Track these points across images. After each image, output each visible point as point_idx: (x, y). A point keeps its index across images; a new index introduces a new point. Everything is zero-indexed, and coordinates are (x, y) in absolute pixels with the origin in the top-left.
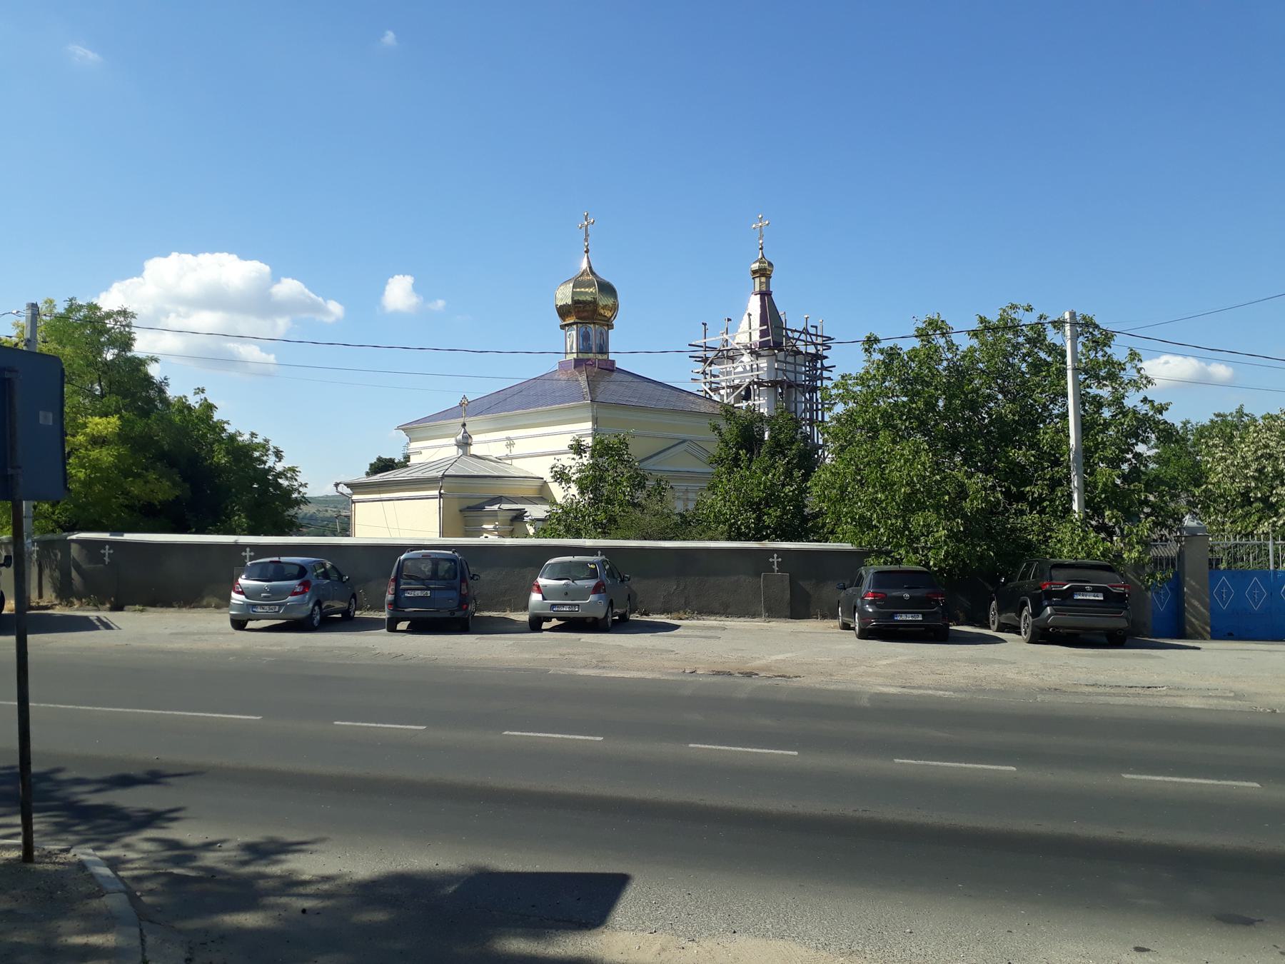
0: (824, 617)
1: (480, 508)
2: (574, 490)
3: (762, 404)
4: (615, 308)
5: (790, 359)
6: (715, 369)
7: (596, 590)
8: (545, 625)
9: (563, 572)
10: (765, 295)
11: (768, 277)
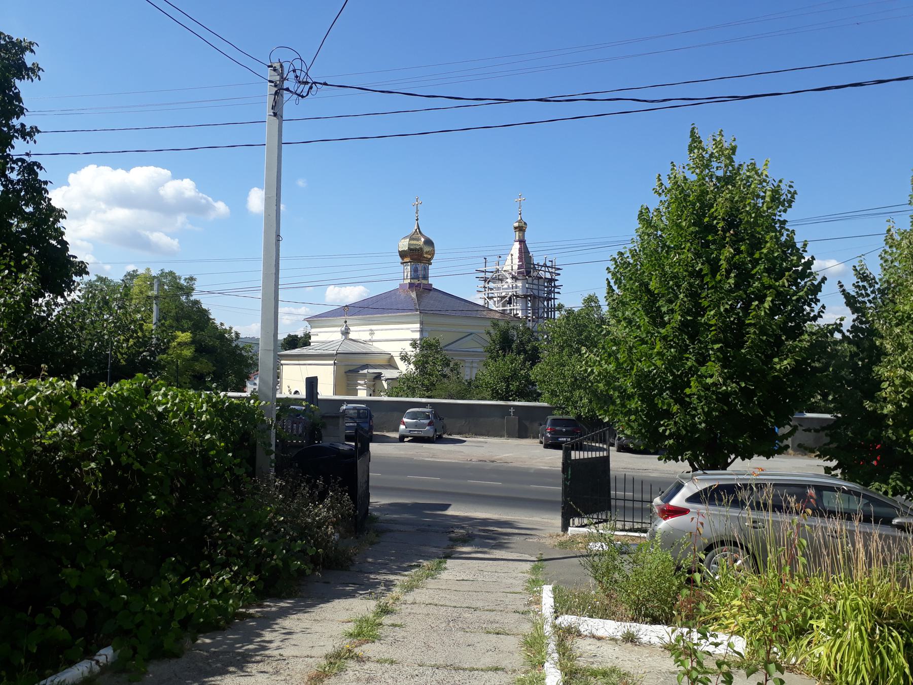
0: (534, 438)
1: (356, 371)
2: (412, 366)
3: (518, 309)
4: (432, 253)
5: (536, 282)
6: (491, 285)
7: (429, 424)
8: (406, 440)
9: (414, 416)
10: (522, 242)
11: (524, 231)
